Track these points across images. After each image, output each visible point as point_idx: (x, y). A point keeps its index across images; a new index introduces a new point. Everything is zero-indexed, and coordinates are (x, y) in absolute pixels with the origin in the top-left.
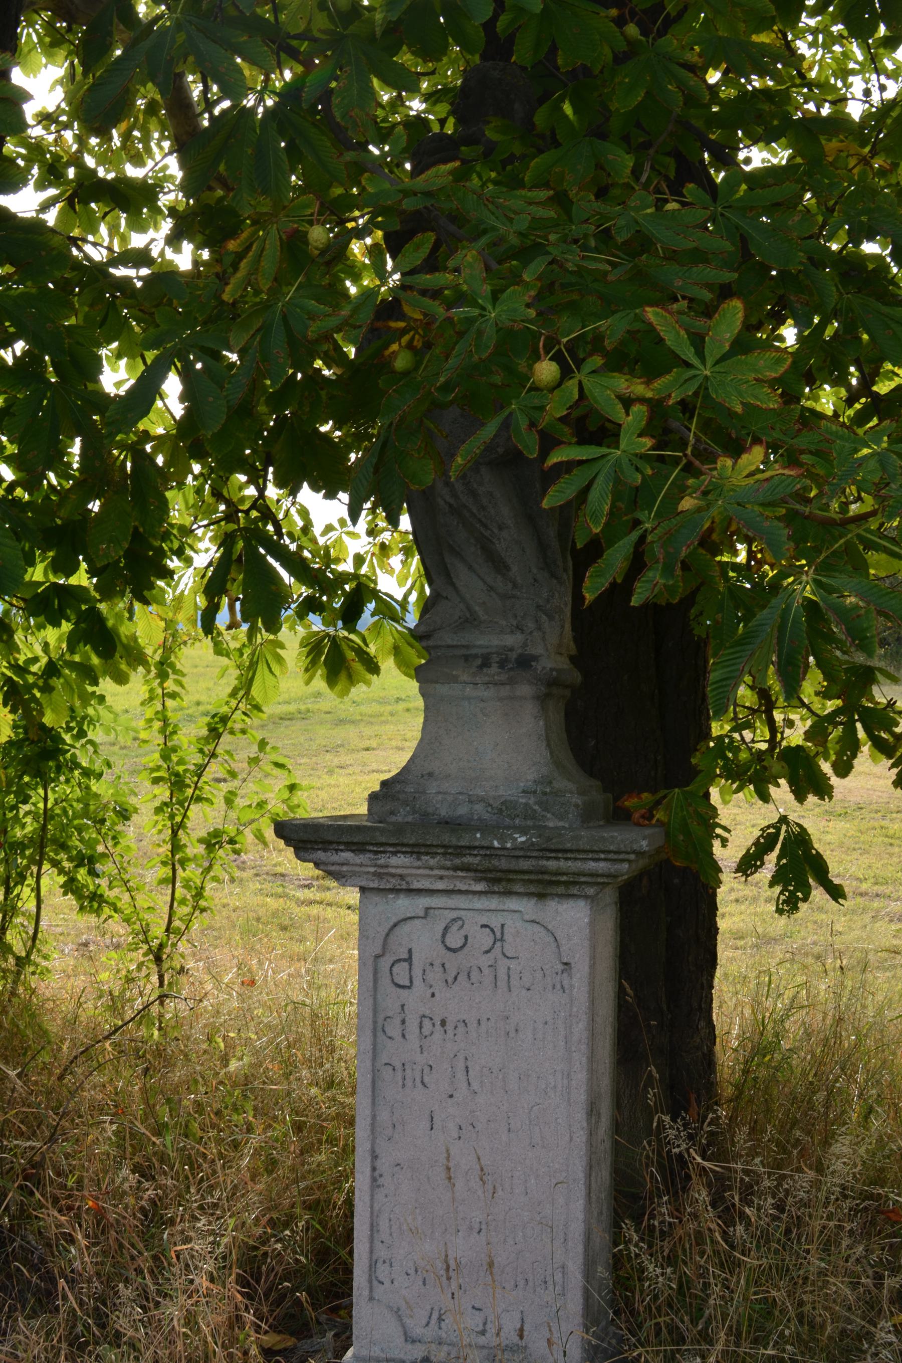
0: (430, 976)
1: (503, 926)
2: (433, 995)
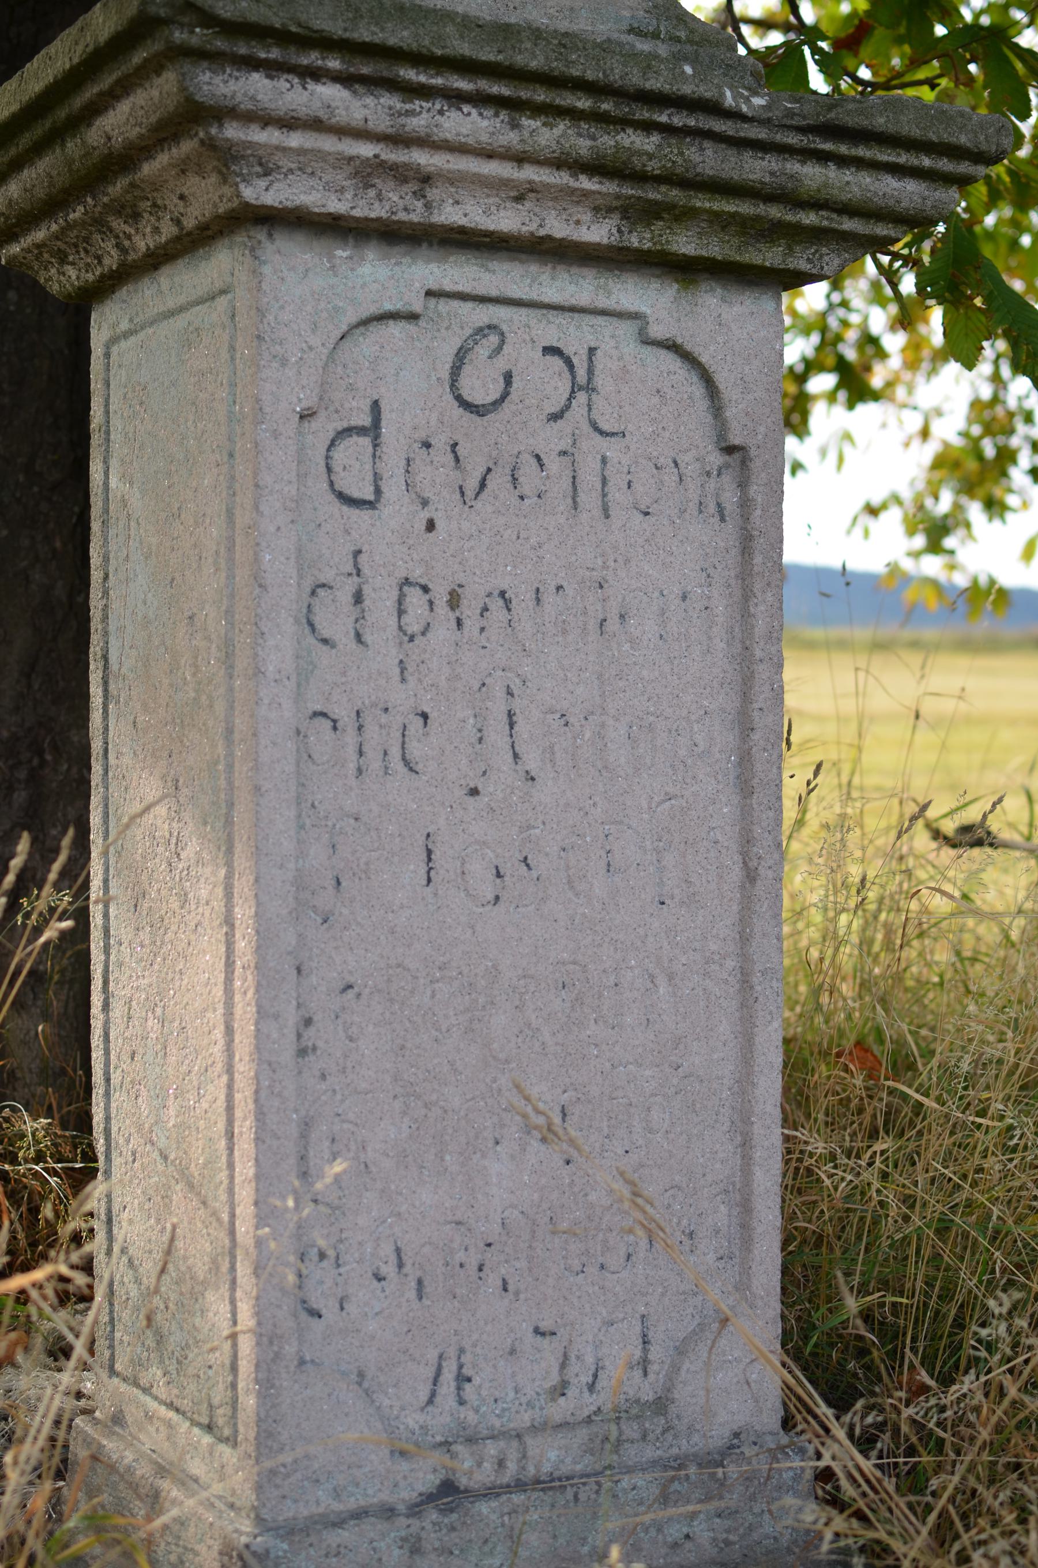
0: (423, 474)
1: (592, 351)
2: (431, 526)
